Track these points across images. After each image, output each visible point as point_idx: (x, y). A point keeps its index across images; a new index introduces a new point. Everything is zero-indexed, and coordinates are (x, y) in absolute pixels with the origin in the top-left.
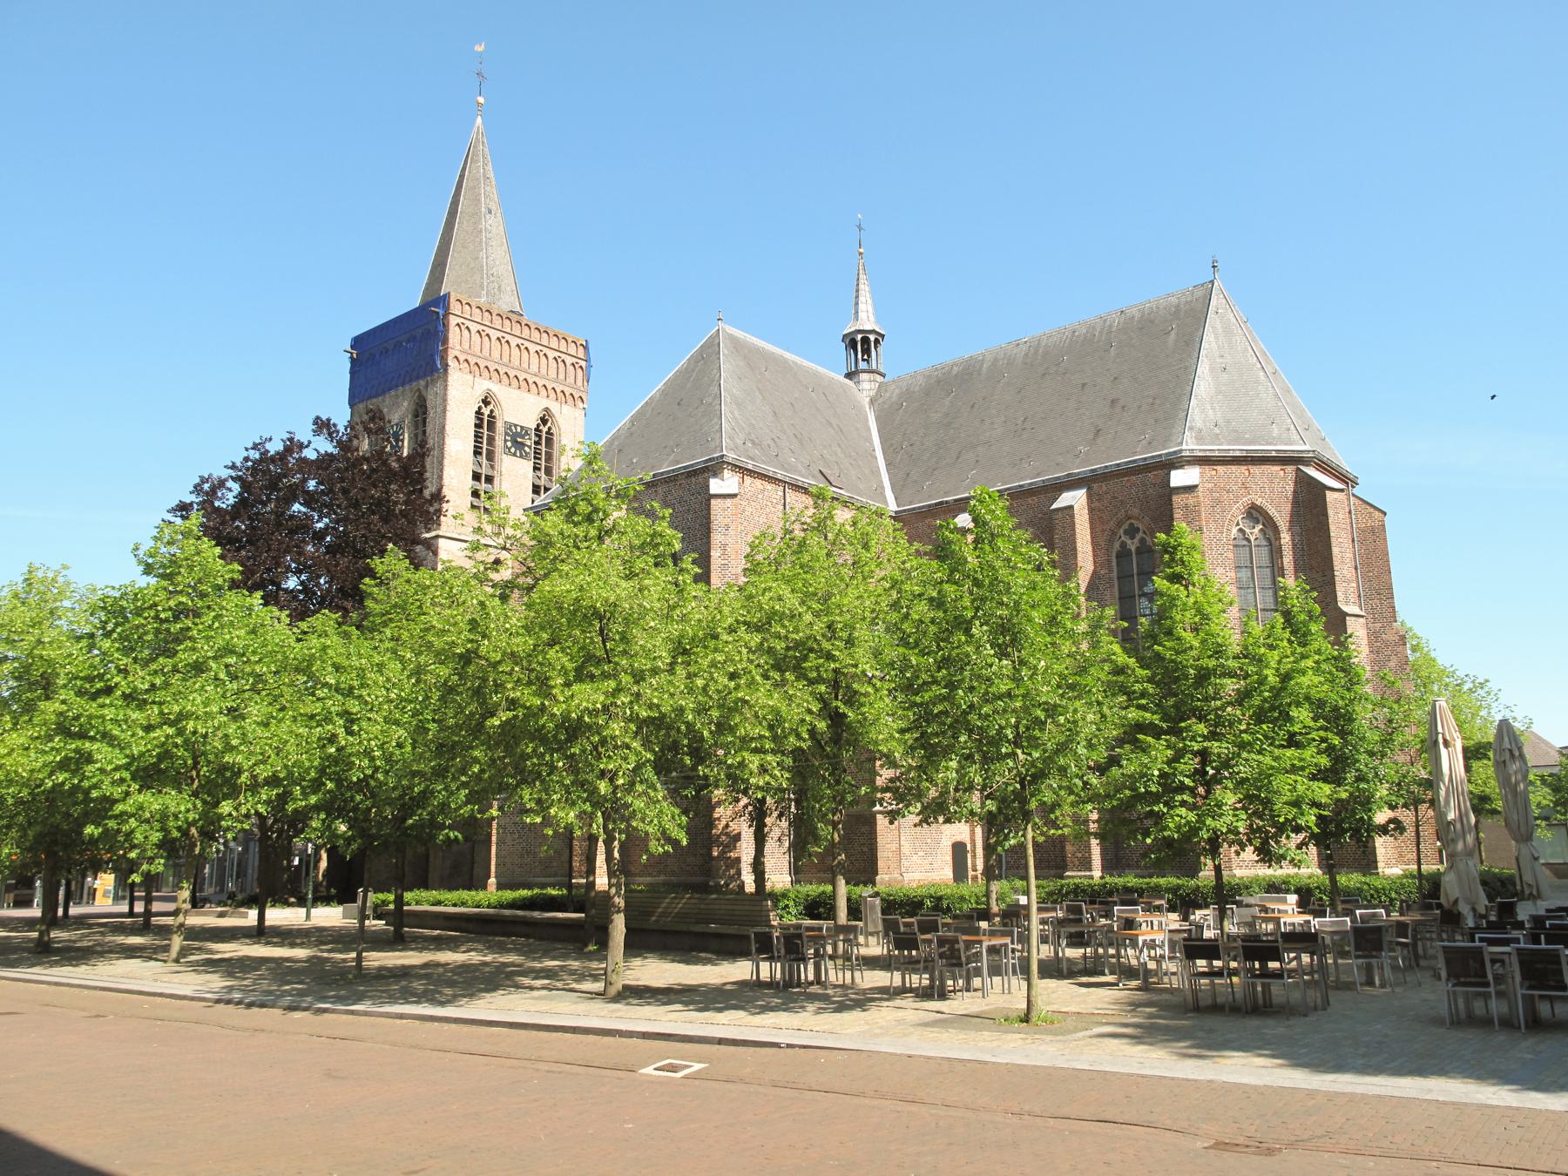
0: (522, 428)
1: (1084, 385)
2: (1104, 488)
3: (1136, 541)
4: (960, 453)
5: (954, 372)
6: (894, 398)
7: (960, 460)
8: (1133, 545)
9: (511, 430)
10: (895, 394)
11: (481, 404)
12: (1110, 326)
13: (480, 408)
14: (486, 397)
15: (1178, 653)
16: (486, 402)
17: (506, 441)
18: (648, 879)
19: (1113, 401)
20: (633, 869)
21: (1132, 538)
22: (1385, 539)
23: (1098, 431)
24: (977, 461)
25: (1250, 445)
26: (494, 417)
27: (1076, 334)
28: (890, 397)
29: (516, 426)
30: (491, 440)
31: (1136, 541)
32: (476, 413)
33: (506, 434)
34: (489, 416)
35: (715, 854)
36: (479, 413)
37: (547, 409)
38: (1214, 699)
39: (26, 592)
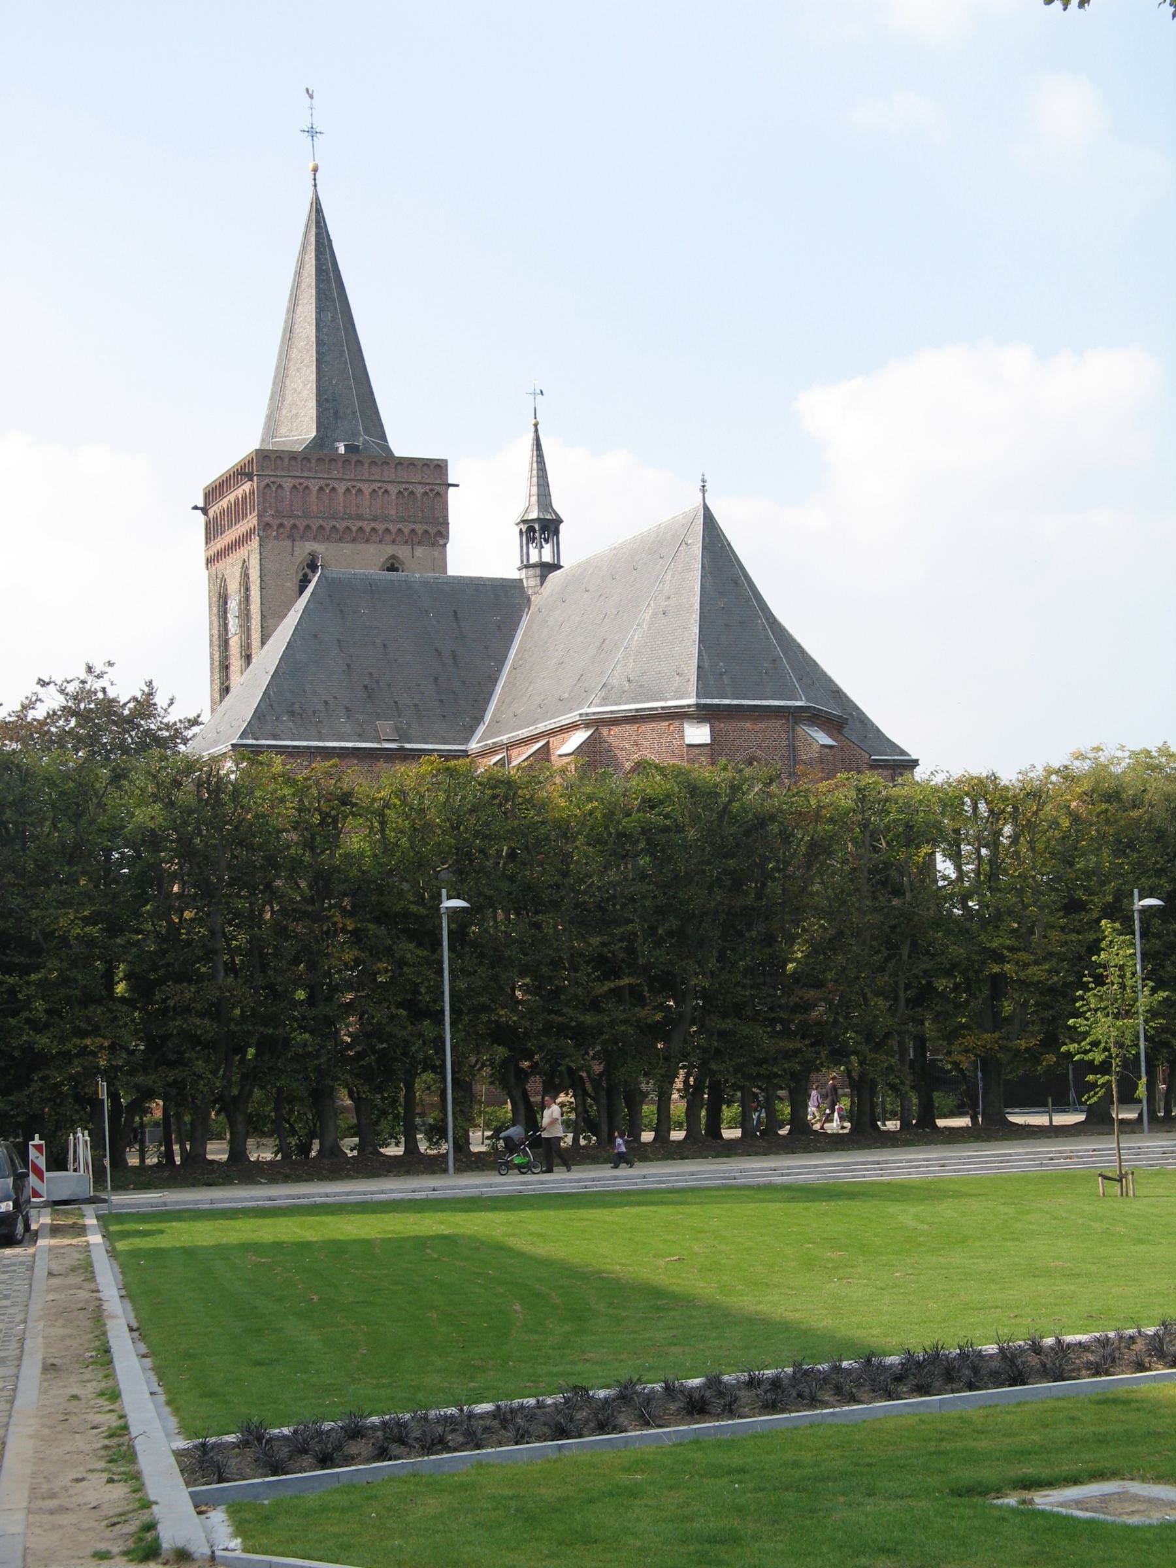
11: (306, 570)
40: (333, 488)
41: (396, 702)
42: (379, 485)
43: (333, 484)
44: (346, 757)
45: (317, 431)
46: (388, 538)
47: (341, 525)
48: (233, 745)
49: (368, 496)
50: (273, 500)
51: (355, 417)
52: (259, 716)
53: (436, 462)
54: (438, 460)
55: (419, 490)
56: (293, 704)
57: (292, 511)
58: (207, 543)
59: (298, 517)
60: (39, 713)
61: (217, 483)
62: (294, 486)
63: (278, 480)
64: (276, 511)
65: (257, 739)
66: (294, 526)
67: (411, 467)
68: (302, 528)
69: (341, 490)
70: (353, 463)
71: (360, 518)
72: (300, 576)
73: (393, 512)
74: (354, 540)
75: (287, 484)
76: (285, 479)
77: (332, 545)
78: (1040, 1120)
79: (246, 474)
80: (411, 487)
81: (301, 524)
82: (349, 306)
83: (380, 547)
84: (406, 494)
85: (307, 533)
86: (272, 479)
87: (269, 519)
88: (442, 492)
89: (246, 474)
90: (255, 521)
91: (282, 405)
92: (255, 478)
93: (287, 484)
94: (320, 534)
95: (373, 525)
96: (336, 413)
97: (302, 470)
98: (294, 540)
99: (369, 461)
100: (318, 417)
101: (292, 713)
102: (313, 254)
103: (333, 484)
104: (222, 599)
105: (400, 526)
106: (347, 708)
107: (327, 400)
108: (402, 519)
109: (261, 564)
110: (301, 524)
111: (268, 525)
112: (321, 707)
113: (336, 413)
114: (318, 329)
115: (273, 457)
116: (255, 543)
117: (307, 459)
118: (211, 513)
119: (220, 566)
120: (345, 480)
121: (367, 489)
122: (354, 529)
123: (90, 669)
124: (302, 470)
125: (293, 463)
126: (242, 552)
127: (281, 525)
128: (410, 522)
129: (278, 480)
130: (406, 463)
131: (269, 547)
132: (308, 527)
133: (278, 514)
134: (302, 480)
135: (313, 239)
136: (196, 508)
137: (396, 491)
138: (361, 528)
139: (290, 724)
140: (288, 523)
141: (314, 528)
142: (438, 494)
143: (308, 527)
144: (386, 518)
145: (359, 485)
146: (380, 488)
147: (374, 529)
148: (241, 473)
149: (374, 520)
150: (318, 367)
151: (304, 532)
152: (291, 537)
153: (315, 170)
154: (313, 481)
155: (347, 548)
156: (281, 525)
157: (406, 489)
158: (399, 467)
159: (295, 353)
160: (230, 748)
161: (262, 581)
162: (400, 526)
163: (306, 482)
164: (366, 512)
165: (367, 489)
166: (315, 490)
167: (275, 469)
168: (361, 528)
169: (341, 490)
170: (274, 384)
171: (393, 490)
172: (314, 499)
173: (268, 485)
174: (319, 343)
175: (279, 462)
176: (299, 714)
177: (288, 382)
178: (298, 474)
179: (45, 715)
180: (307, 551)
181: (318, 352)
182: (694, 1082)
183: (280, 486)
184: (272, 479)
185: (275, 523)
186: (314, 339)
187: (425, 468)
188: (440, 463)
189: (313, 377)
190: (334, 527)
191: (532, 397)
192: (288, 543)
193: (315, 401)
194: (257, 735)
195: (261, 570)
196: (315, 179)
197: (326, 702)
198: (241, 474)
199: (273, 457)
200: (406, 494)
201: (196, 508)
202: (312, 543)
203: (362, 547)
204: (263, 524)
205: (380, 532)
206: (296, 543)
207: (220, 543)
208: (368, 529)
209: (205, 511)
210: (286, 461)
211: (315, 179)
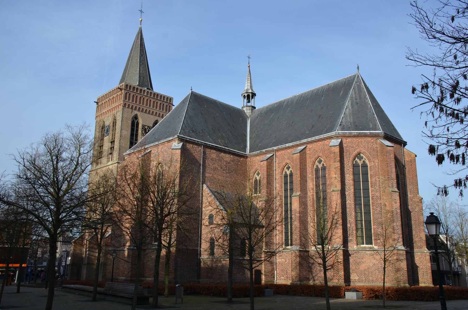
0: (148, 127)
1: (312, 110)
2: (311, 146)
3: (289, 171)
4: (271, 134)
5: (275, 106)
6: (256, 116)
7: (271, 137)
8: (288, 173)
10: (257, 114)
11: (134, 119)
12: (324, 90)
14: (136, 117)
15: (216, 241)
17: (142, 131)
18: (150, 279)
19: (320, 116)
20: (146, 275)
21: (320, 164)
22: (415, 164)
23: (313, 126)
24: (276, 137)
25: (362, 130)
27: (313, 92)
28: (255, 115)
29: (146, 126)
31: (289, 171)
33: (142, 129)
37: (136, 115)
79: (120, 89)
89: (120, 89)
90: (122, 102)
101: (193, 131)
116: (121, 107)
118: (100, 104)
136: (95, 102)
139: (193, 134)
180: (135, 114)
194: (184, 135)
197: (202, 130)
201: (95, 102)
204: (124, 103)
209: (97, 103)
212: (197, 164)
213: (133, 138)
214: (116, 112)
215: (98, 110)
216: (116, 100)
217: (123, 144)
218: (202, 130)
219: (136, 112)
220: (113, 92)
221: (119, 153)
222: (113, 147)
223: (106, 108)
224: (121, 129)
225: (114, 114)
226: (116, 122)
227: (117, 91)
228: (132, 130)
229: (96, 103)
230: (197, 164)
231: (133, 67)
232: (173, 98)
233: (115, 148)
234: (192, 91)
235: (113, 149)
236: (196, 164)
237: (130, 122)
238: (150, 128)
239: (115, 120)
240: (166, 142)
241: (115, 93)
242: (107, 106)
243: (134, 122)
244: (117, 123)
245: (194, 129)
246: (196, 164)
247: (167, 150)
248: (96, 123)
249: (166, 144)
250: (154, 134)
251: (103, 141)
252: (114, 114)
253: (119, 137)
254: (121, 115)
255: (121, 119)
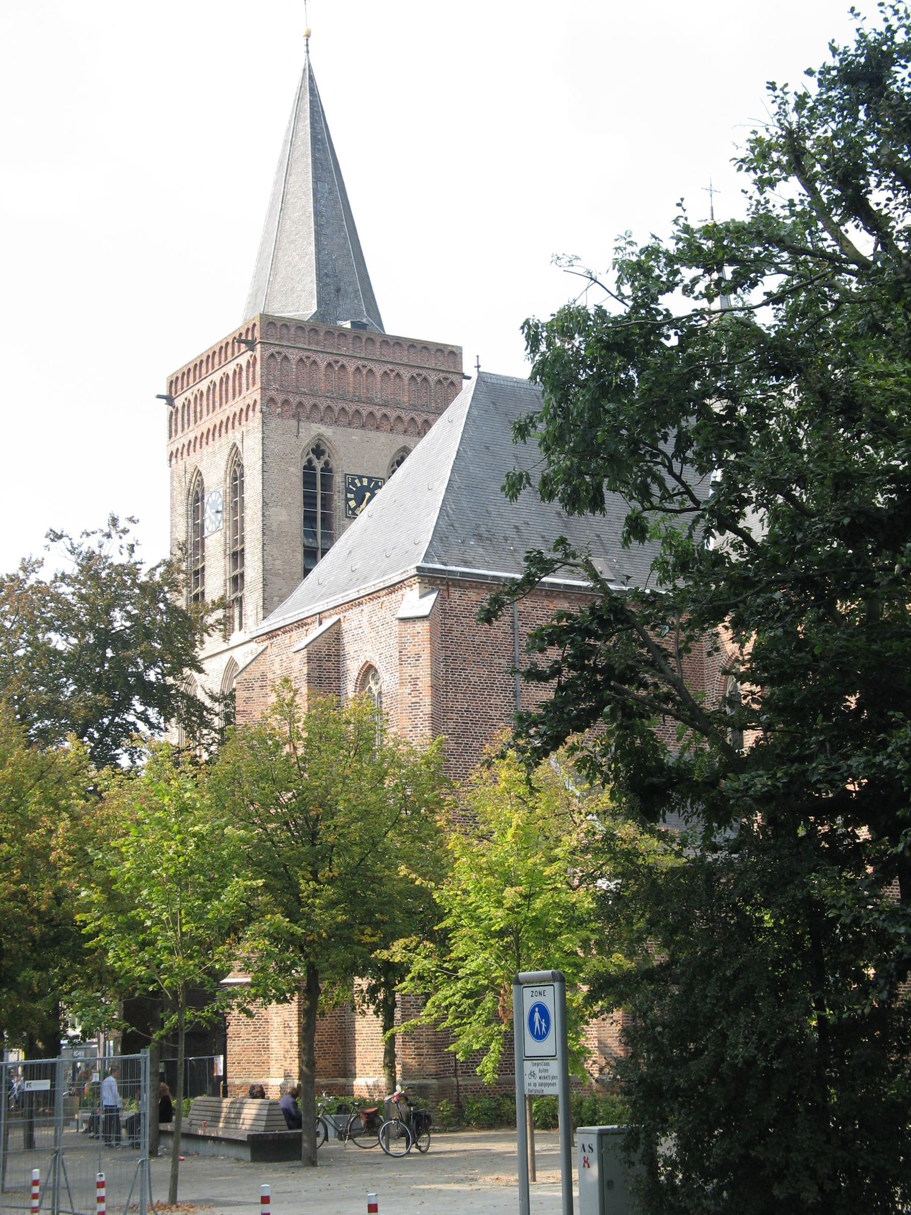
0: (370, 479)
9: (355, 485)
11: (311, 455)
13: (310, 461)
14: (318, 446)
16: (318, 451)
17: (347, 500)
26: (331, 471)
29: (360, 478)
30: (327, 501)
32: (305, 468)
33: (348, 490)
34: (322, 470)
35: (841, 607)
36: (309, 467)
37: (320, 437)
38: (671, 365)
39: (503, 756)
40: (343, 366)
41: (598, 536)
42: (391, 367)
43: (343, 360)
44: (555, 598)
45: (318, 306)
46: (400, 427)
47: (351, 408)
48: (418, 568)
49: (379, 378)
50: (277, 373)
51: (356, 297)
52: (439, 536)
53: (450, 348)
54: (452, 346)
55: (433, 378)
56: (478, 526)
57: (298, 387)
58: (170, 437)
59: (305, 393)
60: (45, 575)
61: (192, 366)
62: (301, 360)
63: (284, 351)
64: (281, 386)
65: (445, 565)
66: (300, 404)
67: (424, 351)
68: (308, 407)
69: (351, 369)
70: (364, 340)
71: (370, 401)
72: (304, 462)
73: (406, 399)
74: (363, 426)
75: (294, 356)
76: (291, 350)
77: (340, 430)
78: (221, 1066)
79: (246, 342)
80: (424, 373)
81: (308, 402)
82: (343, 182)
83: (392, 436)
84: (419, 380)
85: (314, 413)
86: (277, 349)
87: (273, 393)
88: (456, 382)
89: (246, 342)
90: (257, 396)
91: (275, 278)
92: (258, 347)
93: (294, 356)
94: (329, 416)
95: (384, 411)
96: (338, 290)
97: (310, 343)
98: (299, 421)
99: (381, 340)
100: (318, 292)
101: (479, 537)
102: (308, 122)
103: (343, 360)
104: (196, 499)
105: (413, 415)
106: (543, 537)
107: (327, 275)
108: (414, 408)
109: (263, 444)
110: (308, 402)
111: (272, 400)
112: (511, 533)
113: (338, 290)
114: (316, 201)
115: (279, 324)
116: (255, 419)
117: (314, 330)
118: (179, 402)
119: (192, 460)
120: (355, 357)
121: (378, 370)
122: (365, 413)
123: (114, 521)
124: (310, 343)
125: (299, 333)
126: (234, 436)
127: (286, 402)
128: (423, 412)
129: (284, 351)
130: (419, 346)
131: (273, 425)
132: (315, 406)
133: (282, 389)
134: (309, 354)
135: (307, 107)
136: (159, 397)
137: (409, 375)
138: (371, 413)
139: (481, 550)
140: (294, 400)
141: (322, 408)
142: (452, 383)
143: (315, 406)
144: (397, 406)
145: (370, 365)
146: (392, 371)
147: (385, 416)
148: (244, 340)
149: (385, 405)
150: (317, 240)
151: (310, 412)
152: (297, 416)
153: (308, 36)
154: (321, 355)
155: (356, 435)
156: (286, 402)
157: (419, 375)
158: (411, 350)
159: (288, 224)
160: (414, 572)
161: (264, 463)
162: (413, 415)
163: (314, 356)
164: (378, 397)
165: (378, 370)
166: (323, 365)
167: (281, 339)
168: (371, 413)
169: (351, 369)
170: (259, 261)
171: (406, 374)
172: (321, 375)
173: (272, 355)
174: (317, 213)
175: (285, 331)
176: (487, 539)
177: (280, 254)
178: (305, 347)
179: (53, 578)
180: (313, 434)
181: (316, 223)
182: (44, 1044)
183: (286, 358)
184: (277, 349)
185: (280, 398)
186: (311, 210)
187: (438, 354)
188: (454, 350)
189: (312, 249)
190: (343, 409)
191: (709, 193)
192: (294, 422)
193: (314, 275)
194: (445, 560)
195: (263, 451)
196: (307, 45)
197: (516, 527)
198: (240, 341)
199: (279, 324)
200: (419, 380)
201: (159, 397)
202: (318, 425)
203: (373, 434)
204: (267, 398)
205: (392, 420)
206: (302, 424)
207: (182, 439)
208: (378, 415)
209: (170, 400)
210: (293, 329)
211: (307, 45)
212: (501, 661)
213: (315, 533)
214: (239, 436)
215: (173, 427)
216: (237, 388)
217: (277, 562)
218: (516, 527)
219: (315, 429)
220: (221, 352)
221: (264, 599)
222: (242, 575)
223: (201, 418)
224: (265, 504)
225: (235, 444)
226: (242, 475)
227: (236, 350)
228: (309, 500)
229: (164, 401)
230: (501, 661)
231: (292, 242)
232: (460, 348)
233: (247, 578)
234: (479, 373)
235: (243, 584)
236: (497, 661)
237: (296, 473)
238: (377, 483)
239: (240, 465)
240: (384, 592)
241: (230, 358)
242: (205, 412)
243: (314, 469)
244: (247, 479)
245: (483, 529)
246: (497, 661)
247: (387, 620)
248: (172, 478)
249: (385, 599)
250: (350, 552)
251: (203, 551)
252: (235, 444)
253: (260, 535)
254: (259, 447)
255: (260, 462)
